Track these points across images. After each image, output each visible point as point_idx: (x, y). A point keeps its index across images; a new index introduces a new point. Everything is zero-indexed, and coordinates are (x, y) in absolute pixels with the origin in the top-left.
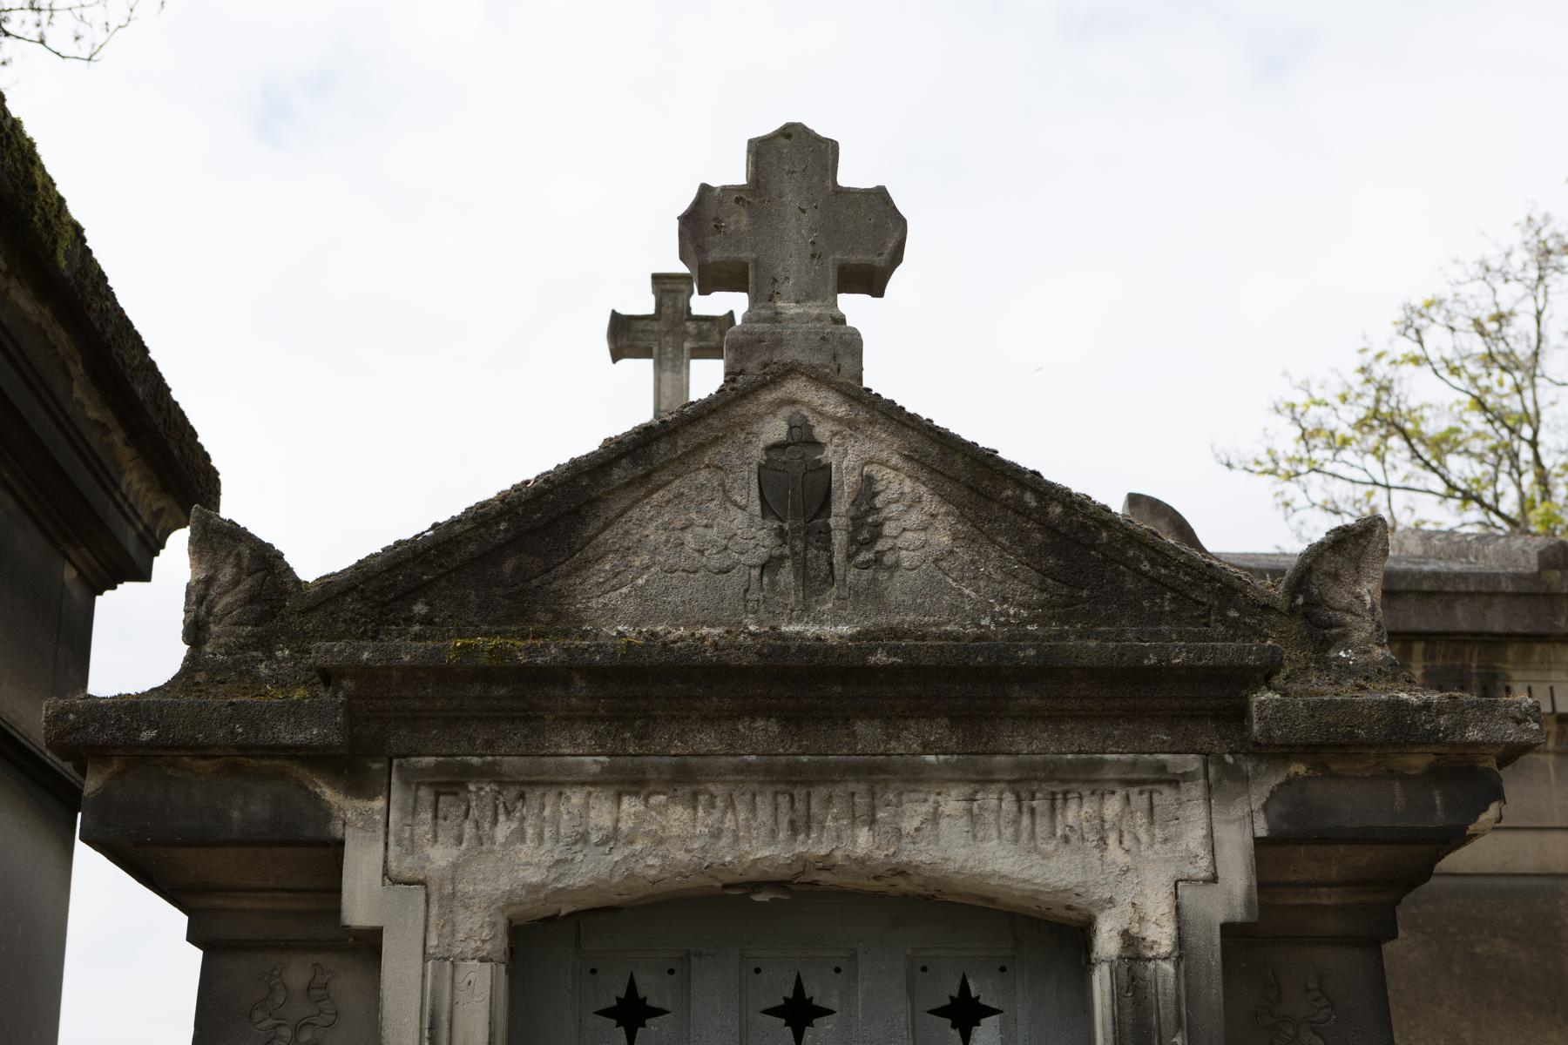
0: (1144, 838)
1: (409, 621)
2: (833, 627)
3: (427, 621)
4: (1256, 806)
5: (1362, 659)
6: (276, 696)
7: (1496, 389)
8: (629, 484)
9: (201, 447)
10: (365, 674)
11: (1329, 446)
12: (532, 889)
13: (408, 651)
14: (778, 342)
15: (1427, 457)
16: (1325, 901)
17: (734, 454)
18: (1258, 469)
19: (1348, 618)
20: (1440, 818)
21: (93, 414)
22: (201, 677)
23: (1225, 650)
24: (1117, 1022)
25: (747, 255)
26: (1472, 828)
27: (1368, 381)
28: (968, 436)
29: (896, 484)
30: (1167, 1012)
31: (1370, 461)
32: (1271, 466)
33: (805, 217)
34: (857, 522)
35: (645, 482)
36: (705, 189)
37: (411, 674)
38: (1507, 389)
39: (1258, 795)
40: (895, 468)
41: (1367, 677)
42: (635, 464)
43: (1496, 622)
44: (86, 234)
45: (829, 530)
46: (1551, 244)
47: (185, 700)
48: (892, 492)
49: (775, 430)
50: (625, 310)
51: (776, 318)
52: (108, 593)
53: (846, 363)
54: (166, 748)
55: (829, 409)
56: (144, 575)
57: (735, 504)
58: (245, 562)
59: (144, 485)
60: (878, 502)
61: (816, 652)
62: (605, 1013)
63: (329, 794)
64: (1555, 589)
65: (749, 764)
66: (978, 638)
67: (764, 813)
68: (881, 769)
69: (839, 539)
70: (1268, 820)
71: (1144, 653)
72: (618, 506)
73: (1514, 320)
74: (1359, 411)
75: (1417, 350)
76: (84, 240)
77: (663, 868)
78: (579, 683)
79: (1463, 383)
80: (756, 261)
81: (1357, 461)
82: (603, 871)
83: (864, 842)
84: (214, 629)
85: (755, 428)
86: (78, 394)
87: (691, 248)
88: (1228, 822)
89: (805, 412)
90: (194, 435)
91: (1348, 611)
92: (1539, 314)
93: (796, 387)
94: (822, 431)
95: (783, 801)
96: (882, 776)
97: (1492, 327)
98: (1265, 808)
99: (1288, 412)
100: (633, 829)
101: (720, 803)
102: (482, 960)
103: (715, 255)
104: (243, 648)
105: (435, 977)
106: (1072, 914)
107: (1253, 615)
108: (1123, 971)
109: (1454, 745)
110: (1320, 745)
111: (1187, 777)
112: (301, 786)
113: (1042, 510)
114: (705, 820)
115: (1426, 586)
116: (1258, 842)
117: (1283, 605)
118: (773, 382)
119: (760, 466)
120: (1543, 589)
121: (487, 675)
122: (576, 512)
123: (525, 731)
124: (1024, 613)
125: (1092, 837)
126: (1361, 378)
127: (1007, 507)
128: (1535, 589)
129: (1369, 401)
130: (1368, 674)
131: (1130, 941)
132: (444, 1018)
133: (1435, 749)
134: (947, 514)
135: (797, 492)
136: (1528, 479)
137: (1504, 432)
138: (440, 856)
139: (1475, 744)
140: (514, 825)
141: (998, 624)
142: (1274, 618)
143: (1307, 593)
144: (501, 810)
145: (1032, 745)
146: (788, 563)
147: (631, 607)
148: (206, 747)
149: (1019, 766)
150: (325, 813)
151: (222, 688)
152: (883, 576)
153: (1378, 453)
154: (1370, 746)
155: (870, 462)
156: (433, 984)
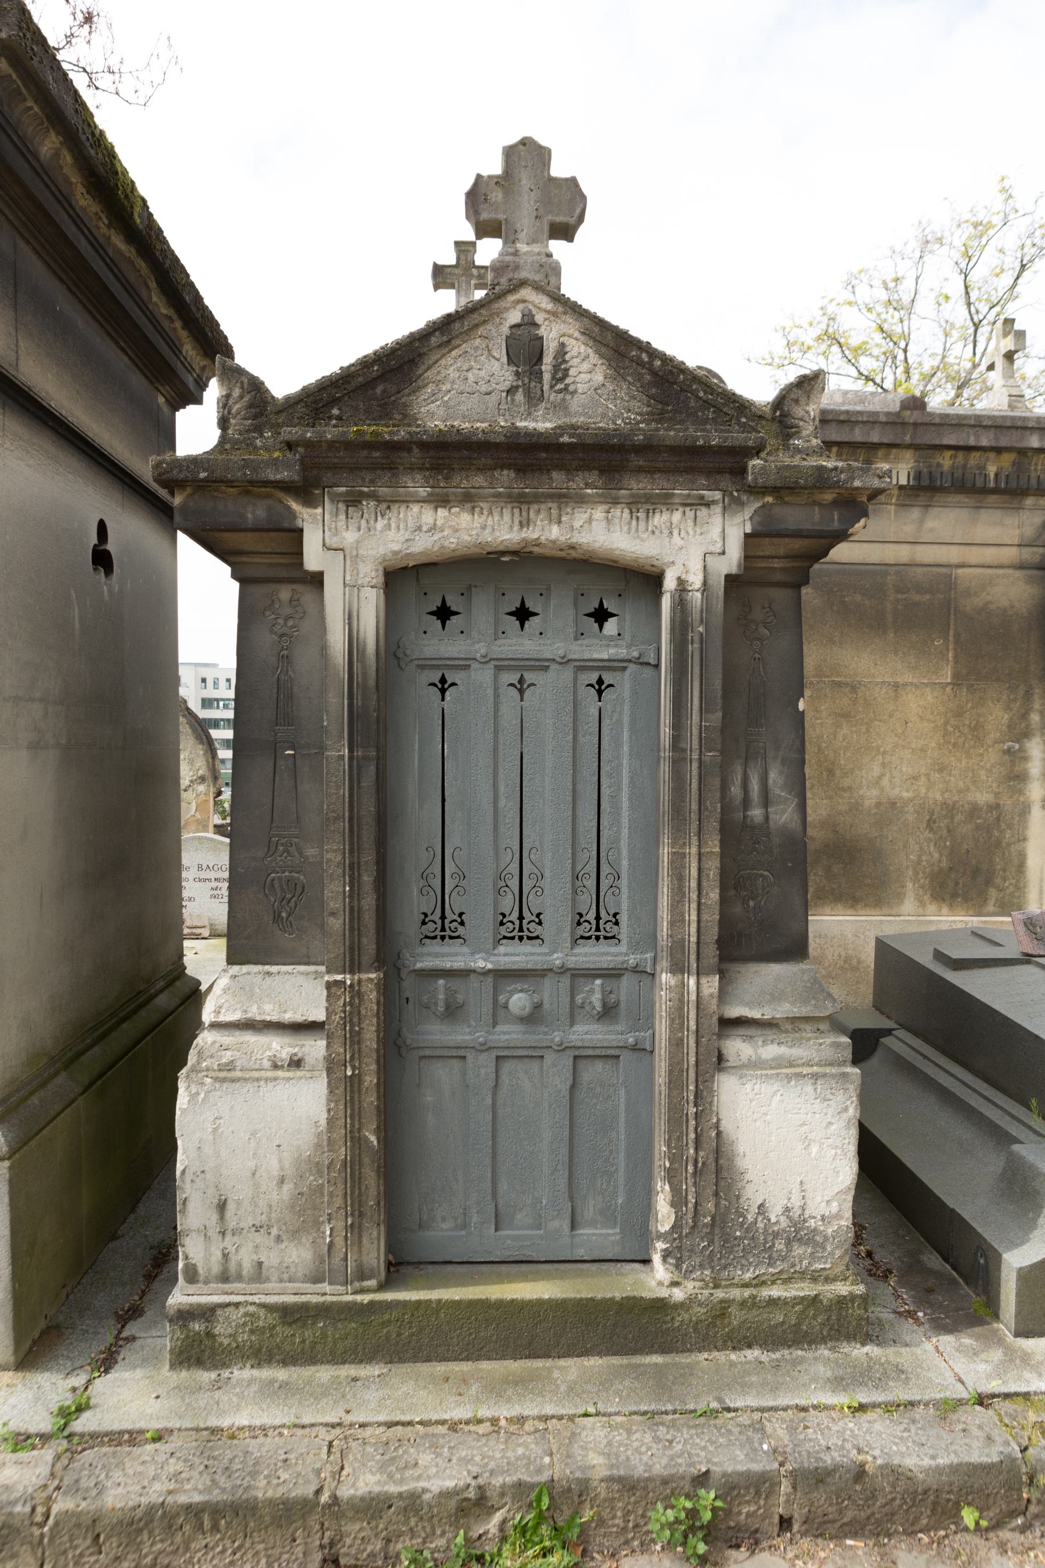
0: (691, 532)
1: (330, 418)
2: (541, 423)
3: (339, 418)
4: (747, 517)
5: (806, 445)
6: (265, 456)
7: (890, 320)
8: (439, 346)
9: (222, 332)
10: (309, 444)
11: (800, 350)
12: (395, 553)
13: (331, 432)
14: (517, 267)
15: (850, 357)
16: (776, 566)
17: (494, 330)
18: (764, 362)
19: (801, 423)
20: (836, 525)
21: (164, 311)
22: (228, 446)
23: (737, 437)
24: (673, 621)
25: (501, 216)
26: (851, 530)
27: (824, 314)
28: (614, 323)
29: (579, 349)
30: (696, 616)
31: (821, 359)
32: (770, 361)
33: (533, 194)
34: (556, 368)
35: (448, 344)
36: (479, 177)
37: (332, 444)
38: (896, 319)
39: (748, 511)
40: (577, 339)
41: (807, 453)
42: (443, 334)
43: (875, 437)
44: (149, 204)
45: (542, 373)
46: (929, 238)
47: (220, 458)
48: (574, 353)
49: (514, 317)
50: (440, 262)
51: (516, 253)
52: (181, 410)
53: (553, 280)
54: (213, 482)
55: (543, 305)
56: (198, 401)
57: (494, 357)
58: (246, 386)
59: (195, 352)
60: (567, 357)
61: (533, 436)
62: (432, 613)
63: (295, 506)
64: (906, 420)
65: (500, 493)
66: (615, 430)
67: (507, 516)
68: (565, 496)
69: (547, 377)
70: (752, 524)
71: (697, 438)
72: (434, 358)
73: (904, 281)
74: (818, 331)
75: (851, 298)
76: (148, 208)
77: (458, 544)
78: (416, 450)
79: (873, 316)
80: (506, 220)
81: (814, 359)
82: (429, 545)
83: (555, 532)
84: (233, 421)
85: (504, 316)
86: (155, 299)
87: (471, 211)
88: (732, 525)
89: (531, 307)
90: (218, 325)
91: (801, 420)
92: (918, 278)
93: (526, 293)
94: (539, 318)
95: (516, 511)
96: (563, 499)
97: (892, 285)
98: (751, 518)
99: (781, 331)
100: (443, 525)
101: (485, 512)
102: (372, 587)
103: (484, 216)
104: (248, 431)
105: (350, 595)
106: (654, 569)
107: (753, 421)
108: (677, 596)
109: (847, 489)
110: (781, 488)
111: (714, 502)
112: (281, 502)
113: (651, 363)
114: (478, 520)
115: (842, 418)
116: (747, 535)
117: (769, 416)
118: (514, 289)
119: (507, 337)
120: (900, 421)
121: (370, 446)
122: (412, 361)
123: (390, 475)
124: (639, 418)
125: (666, 532)
126: (821, 312)
127: (633, 361)
128: (897, 420)
129: (824, 326)
130: (808, 452)
131: (681, 582)
132: (355, 614)
133: (837, 491)
134: (602, 364)
135: (526, 351)
136: (900, 370)
137: (891, 344)
138: (350, 537)
139: (857, 488)
140: (386, 522)
141: (625, 423)
142: (764, 423)
143: (782, 409)
144: (379, 514)
145: (638, 485)
146: (521, 390)
147: (441, 412)
148: (232, 481)
149: (632, 496)
150: (293, 516)
151: (238, 452)
152: (568, 397)
153: (825, 355)
154: (805, 489)
155: (563, 335)
156: (527, 1229)
